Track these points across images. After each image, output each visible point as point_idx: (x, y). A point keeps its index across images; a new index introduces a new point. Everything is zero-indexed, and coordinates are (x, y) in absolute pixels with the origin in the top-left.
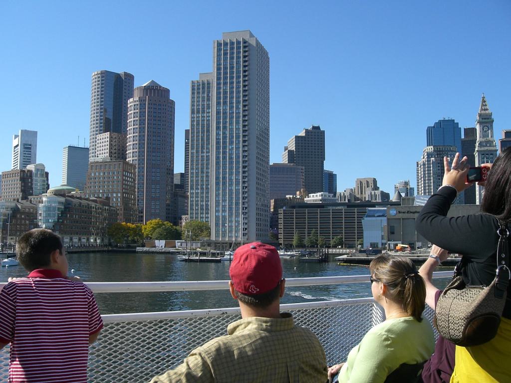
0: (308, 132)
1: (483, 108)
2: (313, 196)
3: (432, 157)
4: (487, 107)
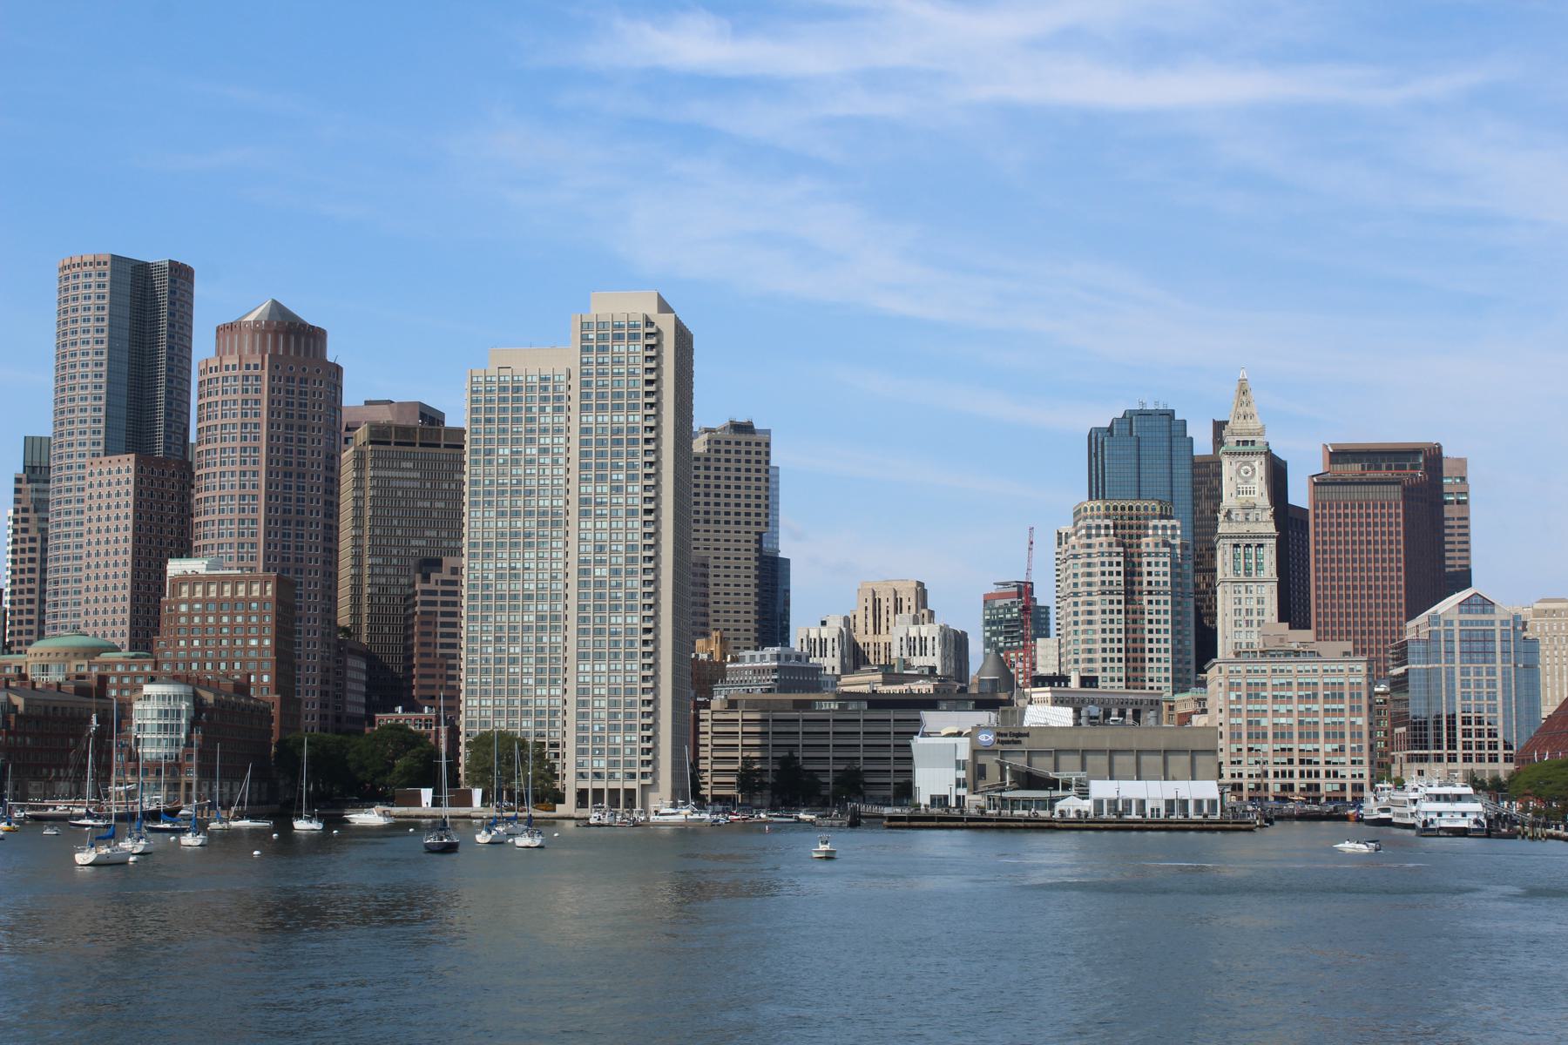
1: (1241, 410)
2: (753, 658)
4: (1253, 409)
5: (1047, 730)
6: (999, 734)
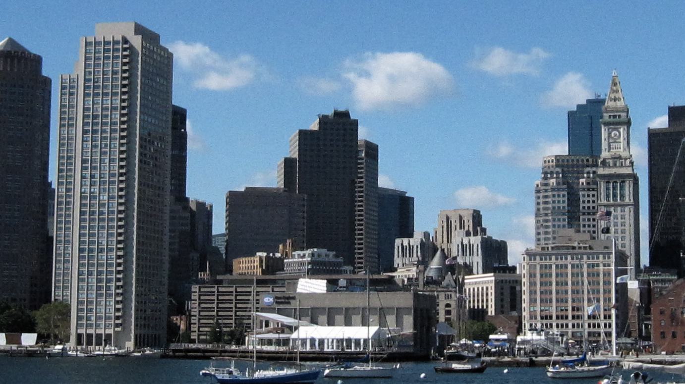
0: (326, 123)
3: (552, 178)
4: (620, 95)
5: (312, 295)
6: (277, 298)
